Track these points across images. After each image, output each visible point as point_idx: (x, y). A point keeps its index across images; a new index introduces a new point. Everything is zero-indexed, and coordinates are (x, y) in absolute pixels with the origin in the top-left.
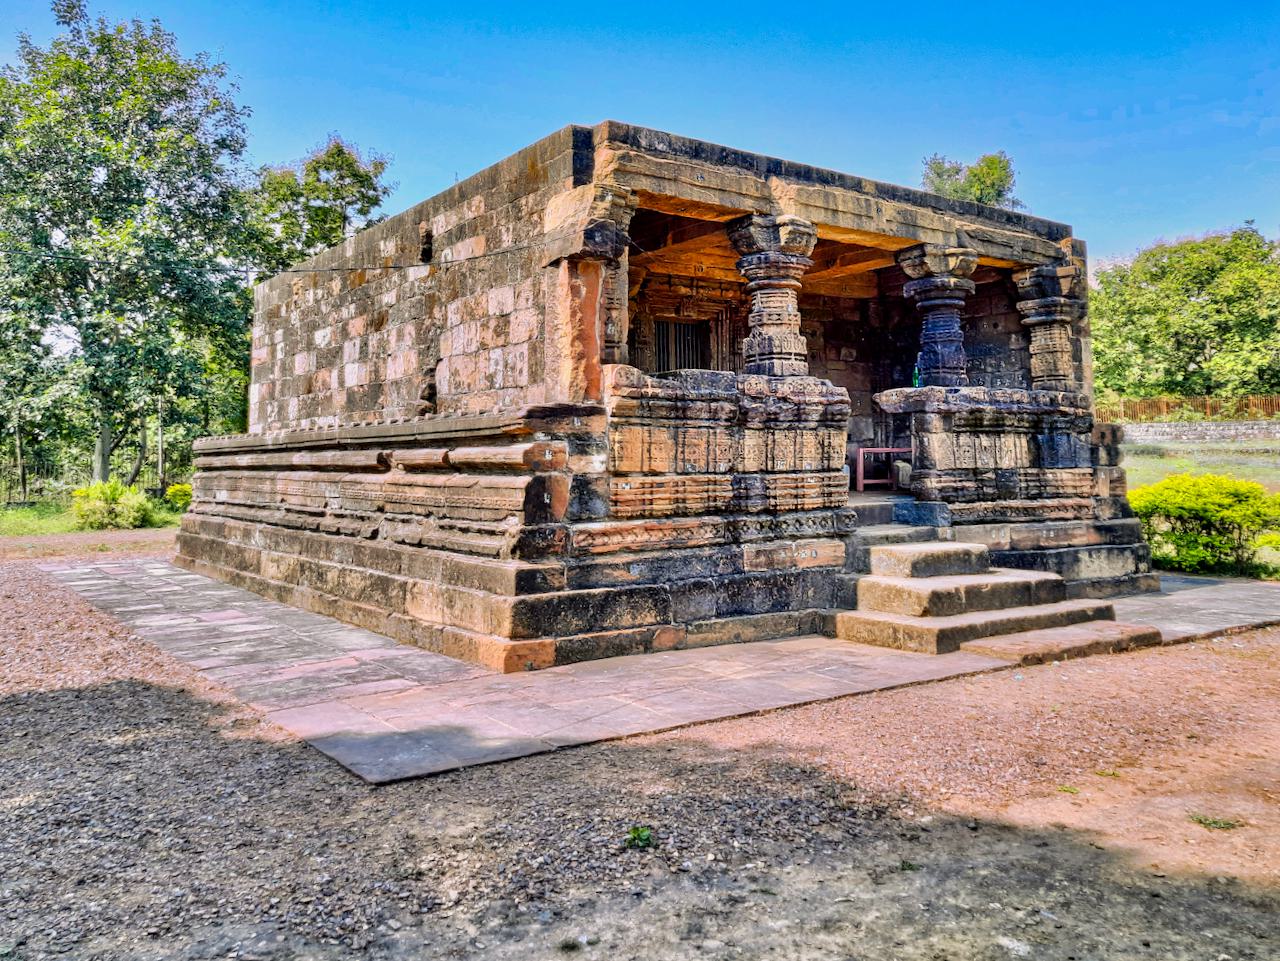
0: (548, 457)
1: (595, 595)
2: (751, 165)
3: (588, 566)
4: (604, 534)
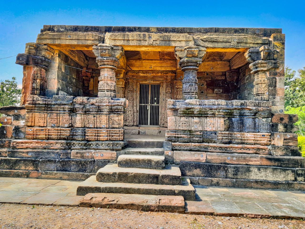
0: (6, 121)
1: (12, 160)
2: (98, 30)
3: (14, 152)
4: (22, 143)
